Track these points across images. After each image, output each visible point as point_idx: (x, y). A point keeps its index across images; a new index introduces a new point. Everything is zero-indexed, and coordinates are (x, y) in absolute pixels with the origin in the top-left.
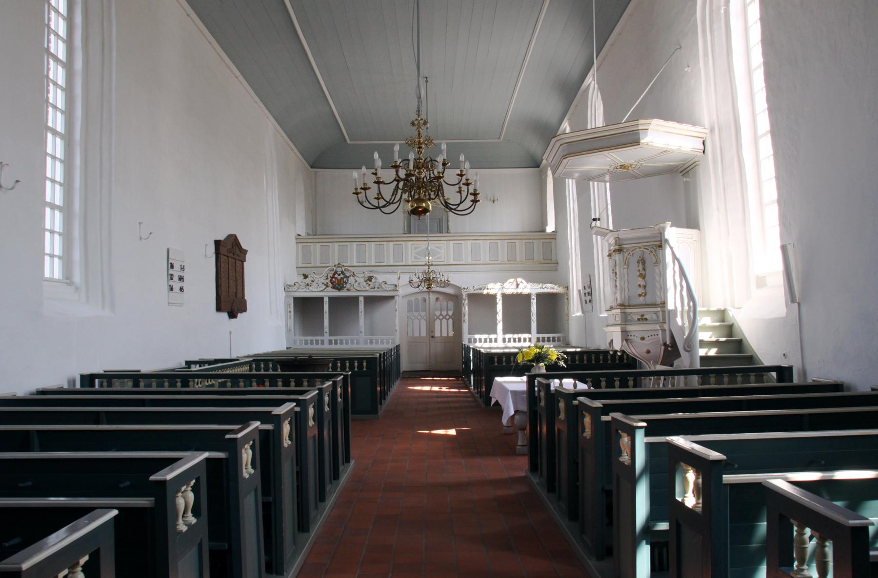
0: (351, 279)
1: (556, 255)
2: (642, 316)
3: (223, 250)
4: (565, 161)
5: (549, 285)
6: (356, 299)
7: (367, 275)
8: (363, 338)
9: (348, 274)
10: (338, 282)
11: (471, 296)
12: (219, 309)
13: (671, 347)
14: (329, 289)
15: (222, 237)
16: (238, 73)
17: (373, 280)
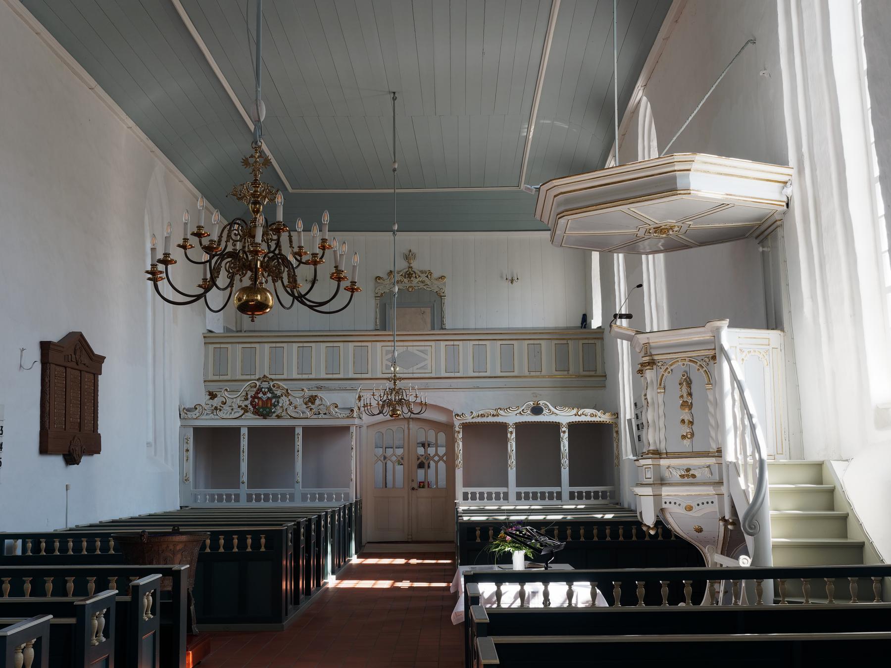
0: (284, 401)
1: (604, 363)
2: (688, 470)
3: (52, 356)
4: (562, 221)
5: (589, 411)
6: (292, 429)
7: (308, 393)
8: (298, 495)
9: (278, 393)
10: (262, 404)
11: (468, 428)
12: (44, 450)
13: (733, 524)
14: (249, 415)
15: (55, 336)
16: (93, 82)
17: (317, 402)
